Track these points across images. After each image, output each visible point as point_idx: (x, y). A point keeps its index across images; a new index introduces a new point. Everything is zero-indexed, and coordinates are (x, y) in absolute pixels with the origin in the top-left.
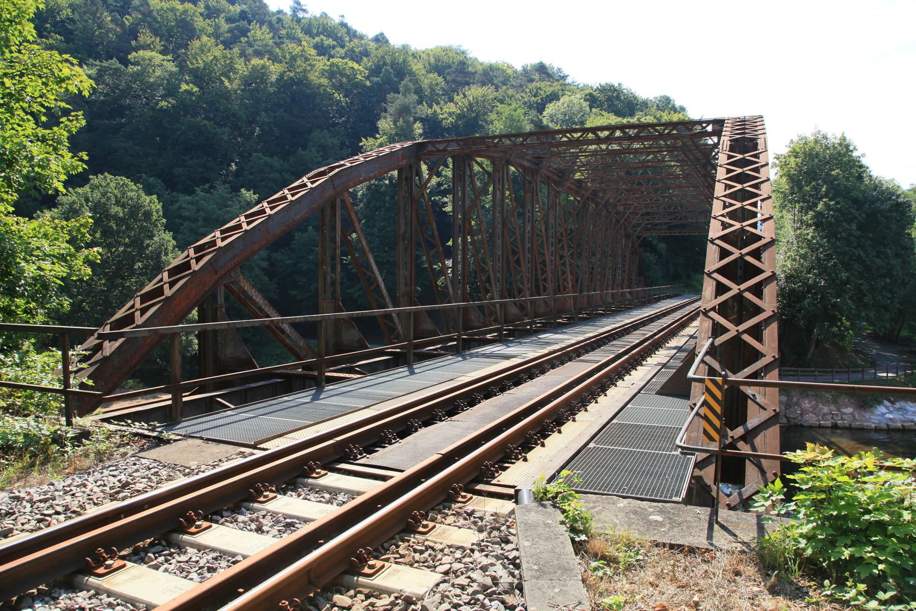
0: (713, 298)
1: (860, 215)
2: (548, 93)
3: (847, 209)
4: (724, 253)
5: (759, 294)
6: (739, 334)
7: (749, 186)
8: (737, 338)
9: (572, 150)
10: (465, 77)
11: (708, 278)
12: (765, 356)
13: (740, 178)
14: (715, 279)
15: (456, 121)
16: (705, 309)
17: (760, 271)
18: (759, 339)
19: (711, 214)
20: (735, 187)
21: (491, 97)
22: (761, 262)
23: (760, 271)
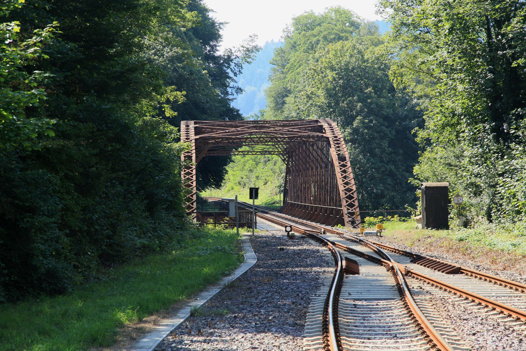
1: (390, 132)
3: (378, 127)
9: (5, 113)
18: (193, 205)
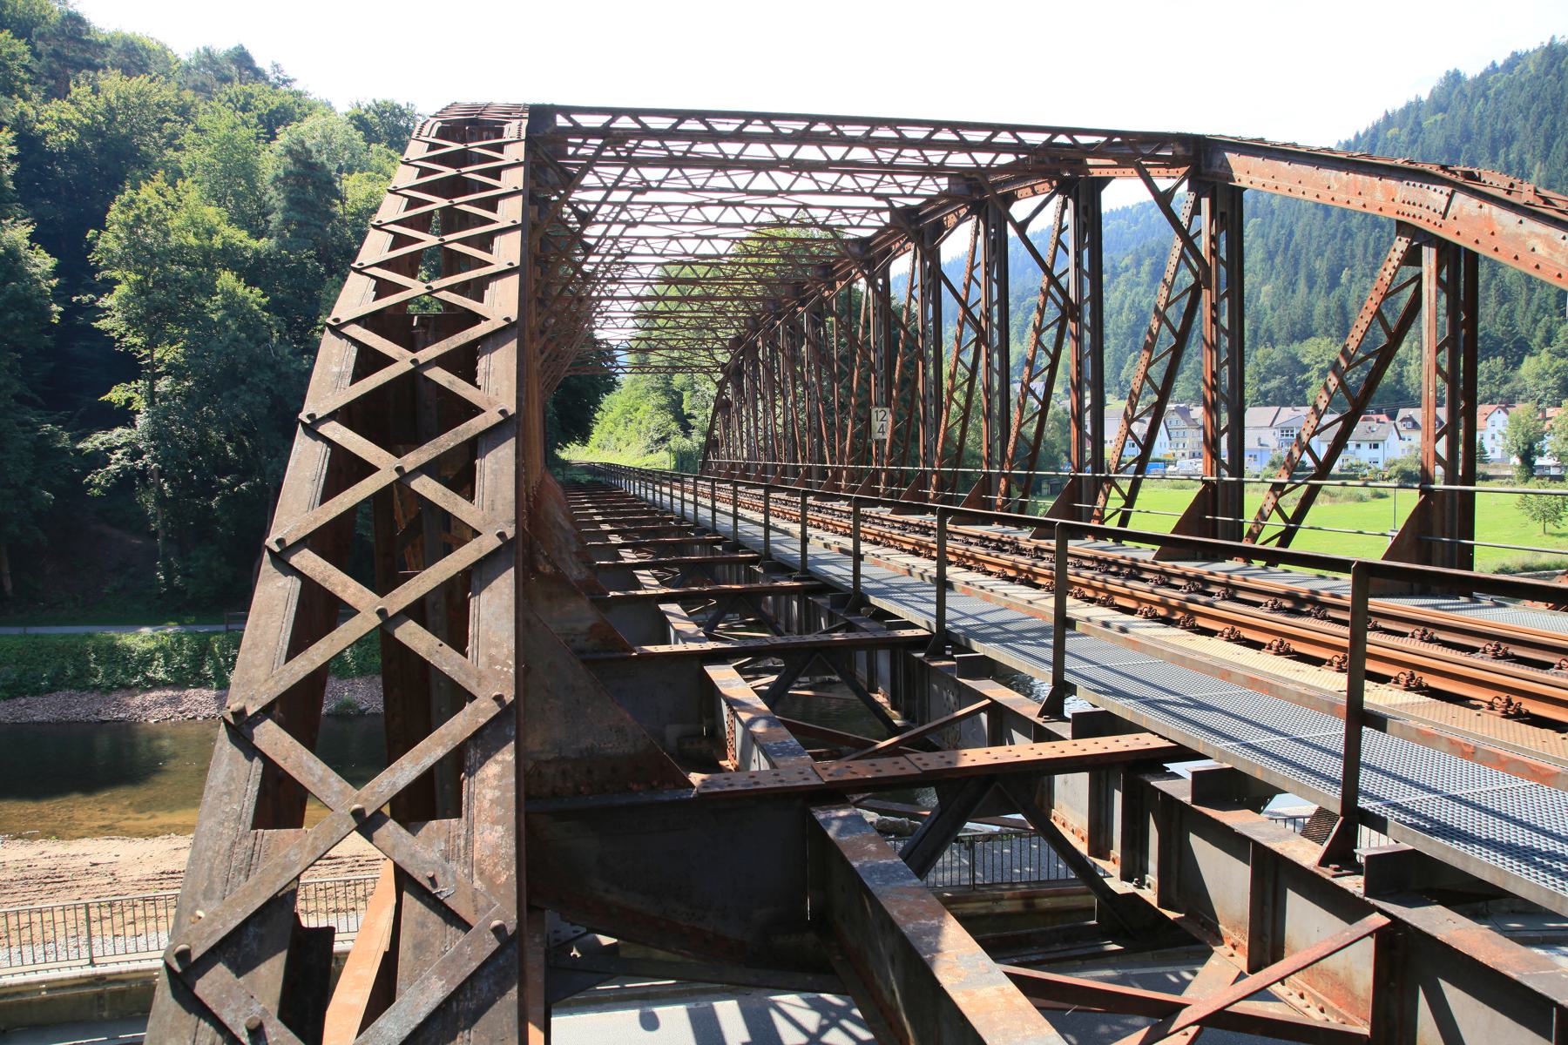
0: (318, 502)
2: (273, 107)
4: (369, 361)
5: (463, 483)
10: (83, 51)
11: (309, 440)
15: (80, 141)
17: (473, 411)
18: (457, 637)
20: (400, 288)
21: (157, 99)
22: (474, 383)
23: (473, 411)
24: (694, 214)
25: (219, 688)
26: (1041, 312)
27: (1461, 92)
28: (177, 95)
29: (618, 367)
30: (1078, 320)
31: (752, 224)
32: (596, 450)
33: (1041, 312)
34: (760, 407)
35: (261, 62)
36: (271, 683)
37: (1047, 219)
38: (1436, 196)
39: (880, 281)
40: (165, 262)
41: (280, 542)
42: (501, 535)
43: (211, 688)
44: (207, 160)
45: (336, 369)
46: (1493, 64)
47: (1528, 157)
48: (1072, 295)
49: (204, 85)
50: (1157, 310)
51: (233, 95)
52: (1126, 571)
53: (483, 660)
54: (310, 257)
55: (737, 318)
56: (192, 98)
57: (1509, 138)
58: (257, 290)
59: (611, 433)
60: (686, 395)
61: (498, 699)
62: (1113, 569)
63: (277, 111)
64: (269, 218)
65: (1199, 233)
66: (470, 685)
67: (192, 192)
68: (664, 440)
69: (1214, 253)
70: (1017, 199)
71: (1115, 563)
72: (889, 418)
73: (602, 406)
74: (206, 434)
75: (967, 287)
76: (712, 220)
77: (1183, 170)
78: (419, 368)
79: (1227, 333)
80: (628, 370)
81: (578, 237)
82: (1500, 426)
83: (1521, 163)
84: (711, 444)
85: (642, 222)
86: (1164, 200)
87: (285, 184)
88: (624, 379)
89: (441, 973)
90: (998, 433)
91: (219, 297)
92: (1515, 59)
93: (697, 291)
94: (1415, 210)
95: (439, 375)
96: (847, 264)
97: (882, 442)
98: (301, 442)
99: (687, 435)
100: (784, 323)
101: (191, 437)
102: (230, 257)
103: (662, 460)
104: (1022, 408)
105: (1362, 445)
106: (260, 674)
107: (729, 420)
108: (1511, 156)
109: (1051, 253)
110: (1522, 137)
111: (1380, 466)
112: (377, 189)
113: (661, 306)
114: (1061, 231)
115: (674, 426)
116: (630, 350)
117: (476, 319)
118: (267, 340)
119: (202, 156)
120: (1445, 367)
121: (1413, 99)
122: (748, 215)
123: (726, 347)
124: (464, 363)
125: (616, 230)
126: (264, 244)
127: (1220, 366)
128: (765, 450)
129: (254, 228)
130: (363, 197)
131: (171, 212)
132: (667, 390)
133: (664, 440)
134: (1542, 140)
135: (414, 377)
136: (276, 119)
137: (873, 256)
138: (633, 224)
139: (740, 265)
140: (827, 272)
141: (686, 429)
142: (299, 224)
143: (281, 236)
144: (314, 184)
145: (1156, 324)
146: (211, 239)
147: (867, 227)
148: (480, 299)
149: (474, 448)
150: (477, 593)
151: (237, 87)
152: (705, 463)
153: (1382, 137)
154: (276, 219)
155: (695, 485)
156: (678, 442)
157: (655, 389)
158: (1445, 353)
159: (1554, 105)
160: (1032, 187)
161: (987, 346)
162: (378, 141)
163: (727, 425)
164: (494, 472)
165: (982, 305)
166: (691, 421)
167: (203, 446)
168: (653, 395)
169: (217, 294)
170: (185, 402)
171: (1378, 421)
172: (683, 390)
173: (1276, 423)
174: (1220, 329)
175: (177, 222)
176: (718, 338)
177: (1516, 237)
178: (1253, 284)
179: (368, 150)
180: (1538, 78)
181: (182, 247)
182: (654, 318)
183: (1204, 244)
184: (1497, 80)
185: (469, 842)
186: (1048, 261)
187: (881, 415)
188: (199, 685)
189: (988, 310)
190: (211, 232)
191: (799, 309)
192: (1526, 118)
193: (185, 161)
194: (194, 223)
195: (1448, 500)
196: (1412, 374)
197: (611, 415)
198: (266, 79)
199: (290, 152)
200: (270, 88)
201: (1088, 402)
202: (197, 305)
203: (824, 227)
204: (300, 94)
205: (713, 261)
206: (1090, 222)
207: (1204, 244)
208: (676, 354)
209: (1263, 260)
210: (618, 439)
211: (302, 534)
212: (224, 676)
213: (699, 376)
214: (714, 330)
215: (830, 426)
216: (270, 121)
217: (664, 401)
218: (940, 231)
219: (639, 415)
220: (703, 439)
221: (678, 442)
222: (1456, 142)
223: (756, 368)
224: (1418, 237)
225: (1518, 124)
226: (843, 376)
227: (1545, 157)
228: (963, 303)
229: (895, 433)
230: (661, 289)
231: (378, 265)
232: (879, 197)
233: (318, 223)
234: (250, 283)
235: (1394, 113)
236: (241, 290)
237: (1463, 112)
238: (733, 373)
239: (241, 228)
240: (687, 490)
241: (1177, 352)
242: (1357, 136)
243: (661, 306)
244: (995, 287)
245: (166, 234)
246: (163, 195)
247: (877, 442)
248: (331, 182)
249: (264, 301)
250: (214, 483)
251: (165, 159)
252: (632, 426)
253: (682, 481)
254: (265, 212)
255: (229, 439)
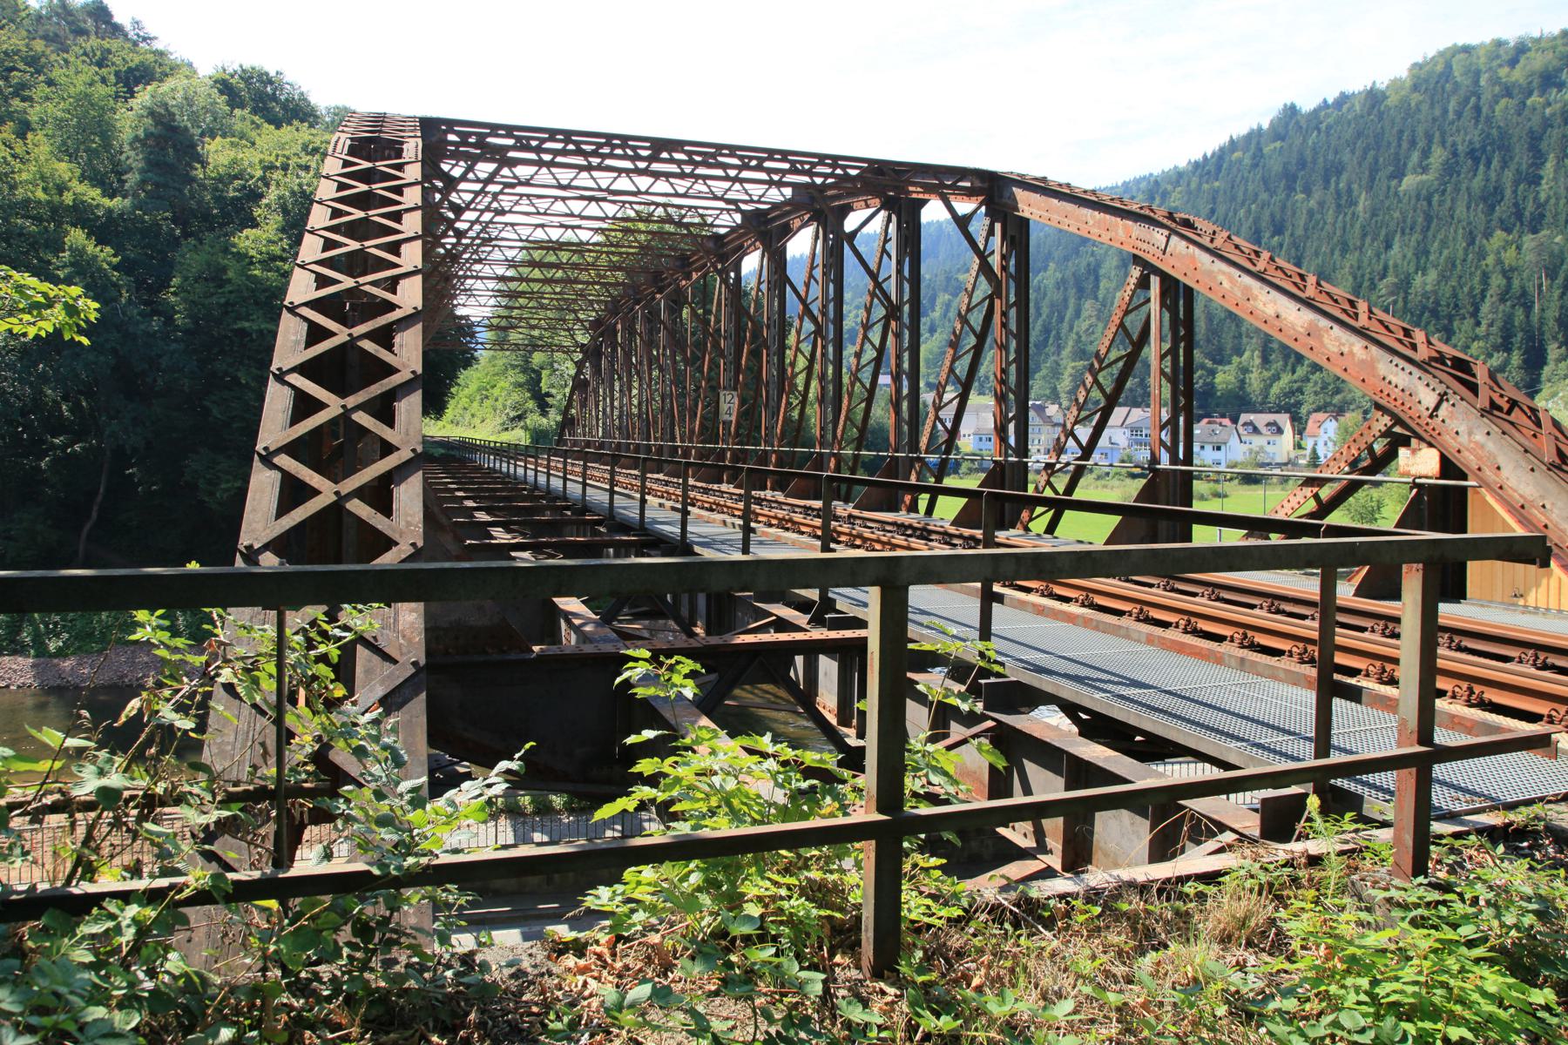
2: (132, 65)
4: (316, 334)
5: (383, 504)
6: (341, 499)
7: (376, 247)
8: (337, 508)
11: (278, 386)
12: (398, 449)
13: (357, 230)
14: (305, 319)
16: (279, 369)
18: (386, 508)
19: (306, 224)
20: (336, 282)
22: (393, 352)
23: (391, 370)
24: (559, 207)
25: (36, 656)
26: (868, 310)
27: (1297, 123)
28: (27, 45)
29: (477, 343)
30: (898, 319)
31: (614, 218)
32: (449, 426)
33: (868, 310)
34: (617, 388)
35: (121, 17)
36: (268, 531)
37: (876, 225)
38: (1159, 236)
39: (732, 275)
40: (11, 215)
41: (266, 449)
42: (414, 450)
43: (28, 656)
44: (60, 114)
45: (293, 338)
46: (1325, 101)
47: (1355, 186)
48: (893, 298)
49: (56, 35)
50: (959, 314)
51: (89, 49)
52: (918, 533)
53: (403, 524)
54: (166, 219)
55: (598, 302)
56: (43, 48)
57: (1339, 169)
58: (108, 249)
59: (465, 409)
60: (545, 373)
61: (413, 545)
62: (909, 532)
63: (137, 68)
64: (124, 177)
65: (993, 252)
66: (395, 537)
67: (41, 146)
68: (520, 417)
69: (1004, 268)
70: (852, 209)
71: (910, 526)
72: (736, 401)
73: (459, 381)
74: (41, 392)
75: (807, 285)
76: (576, 213)
77: (981, 198)
78: (353, 340)
79: (1015, 336)
80: (488, 346)
81: (450, 224)
82: (1331, 433)
83: (1350, 191)
84: (568, 423)
85: (510, 212)
86: (962, 222)
87: (144, 145)
88: (483, 355)
89: (382, 682)
90: (830, 417)
91: (68, 253)
92: (1343, 99)
93: (560, 274)
94: (1145, 246)
95: (367, 345)
96: (701, 258)
97: (727, 424)
98: (273, 387)
99: (544, 414)
100: (643, 308)
101: (23, 395)
102: (81, 215)
103: (519, 436)
104: (850, 395)
105: (1206, 447)
106: (260, 526)
107: (586, 398)
108: (1341, 185)
109: (877, 260)
110: (1349, 168)
111: (1222, 468)
112: (241, 156)
113: (523, 287)
114: (886, 241)
115: (531, 404)
116: (491, 327)
117: (392, 307)
118: (115, 300)
119: (54, 110)
120: (1168, 370)
121: (1255, 127)
122: (611, 209)
123: (585, 328)
124: (384, 337)
125: (487, 217)
126: (117, 203)
127: (1009, 364)
128: (620, 428)
129: (107, 187)
130: (226, 163)
131: (18, 166)
132: (526, 368)
133: (520, 417)
134: (1367, 173)
135: (350, 345)
136: (135, 77)
137: (725, 250)
138: (502, 212)
139: (602, 253)
140: (684, 264)
141: (543, 408)
142: (157, 185)
143: (135, 195)
144: (174, 146)
145: (959, 327)
146: (61, 195)
147: (726, 222)
148: (394, 292)
149: (391, 396)
150: (398, 484)
151: (93, 42)
152: (561, 441)
153: (1227, 159)
154: (132, 179)
155: (549, 460)
156: (535, 419)
157: (514, 367)
158: (1168, 361)
159: (1377, 143)
160: (866, 201)
161: (823, 338)
162: (242, 107)
163: (584, 404)
164: (407, 411)
165: (819, 303)
166: (549, 400)
167: (37, 403)
168: (511, 372)
169: (64, 251)
170: (21, 359)
171: (1221, 424)
172: (542, 368)
173: (1127, 422)
174: (1009, 332)
175: (25, 176)
176: (578, 320)
177: (1210, 273)
178: (1107, 289)
179: (231, 114)
180: (1362, 117)
181: (27, 201)
182: (516, 297)
183: (995, 261)
184: (1327, 116)
185: (396, 620)
186: (873, 267)
187: (729, 398)
188: (14, 653)
189: (824, 306)
190: (61, 188)
191: (658, 296)
192: (1353, 152)
193: (34, 114)
194: (43, 178)
195: (1171, 479)
196: (1253, 381)
197: (466, 391)
198: (126, 36)
199: (152, 113)
200: (129, 45)
201: (905, 391)
202: (40, 260)
203: (680, 224)
204: (161, 54)
205: (579, 248)
206: (910, 237)
207: (995, 261)
208: (536, 333)
209: (1117, 267)
210: (473, 416)
211: (280, 445)
212: (44, 643)
213: (558, 356)
214: (575, 312)
215: (681, 406)
216: (127, 79)
217: (522, 378)
218: (787, 232)
219: (496, 392)
220: (559, 418)
221: (535, 419)
222: (1293, 168)
223: (614, 350)
224: (1148, 269)
225: (1346, 157)
226: (695, 361)
227: (1370, 188)
228: (803, 301)
229: (741, 415)
230: (525, 271)
231: (316, 263)
232: (728, 201)
233: (176, 185)
234: (100, 242)
235: (1238, 138)
236: (91, 248)
237: (1298, 142)
238: (591, 353)
239: (93, 186)
240: (541, 465)
241: (978, 351)
242: (1205, 156)
243: (523, 287)
244: (831, 286)
245: (13, 187)
246: (11, 148)
247: (724, 423)
248: (193, 146)
249: (115, 260)
250: (44, 442)
251: (11, 109)
252: (487, 403)
253: (536, 457)
254: (120, 171)
255: (65, 398)
